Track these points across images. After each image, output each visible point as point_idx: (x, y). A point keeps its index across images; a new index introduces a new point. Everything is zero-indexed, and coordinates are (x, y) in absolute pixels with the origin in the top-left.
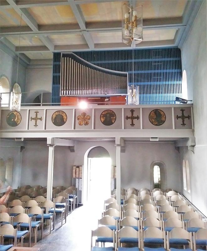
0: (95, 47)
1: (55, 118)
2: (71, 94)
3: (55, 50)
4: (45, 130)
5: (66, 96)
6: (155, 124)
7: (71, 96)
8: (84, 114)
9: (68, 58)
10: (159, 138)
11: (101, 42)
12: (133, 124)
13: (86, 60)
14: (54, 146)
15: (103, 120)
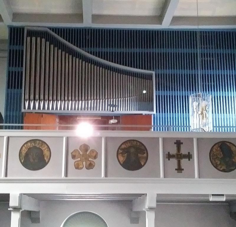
0: (93, 22)
1: (27, 155)
2: (44, 108)
3: (13, 21)
4: (67, 178)
5: (34, 111)
6: (221, 169)
7: (44, 111)
8: (85, 147)
9: (39, 39)
10: (227, 196)
11: (106, 12)
12: (180, 169)
13: (74, 45)
14: (21, 211)
15: (122, 159)
